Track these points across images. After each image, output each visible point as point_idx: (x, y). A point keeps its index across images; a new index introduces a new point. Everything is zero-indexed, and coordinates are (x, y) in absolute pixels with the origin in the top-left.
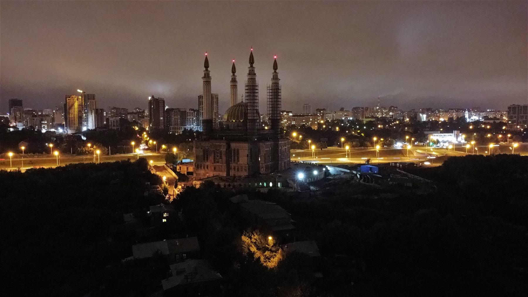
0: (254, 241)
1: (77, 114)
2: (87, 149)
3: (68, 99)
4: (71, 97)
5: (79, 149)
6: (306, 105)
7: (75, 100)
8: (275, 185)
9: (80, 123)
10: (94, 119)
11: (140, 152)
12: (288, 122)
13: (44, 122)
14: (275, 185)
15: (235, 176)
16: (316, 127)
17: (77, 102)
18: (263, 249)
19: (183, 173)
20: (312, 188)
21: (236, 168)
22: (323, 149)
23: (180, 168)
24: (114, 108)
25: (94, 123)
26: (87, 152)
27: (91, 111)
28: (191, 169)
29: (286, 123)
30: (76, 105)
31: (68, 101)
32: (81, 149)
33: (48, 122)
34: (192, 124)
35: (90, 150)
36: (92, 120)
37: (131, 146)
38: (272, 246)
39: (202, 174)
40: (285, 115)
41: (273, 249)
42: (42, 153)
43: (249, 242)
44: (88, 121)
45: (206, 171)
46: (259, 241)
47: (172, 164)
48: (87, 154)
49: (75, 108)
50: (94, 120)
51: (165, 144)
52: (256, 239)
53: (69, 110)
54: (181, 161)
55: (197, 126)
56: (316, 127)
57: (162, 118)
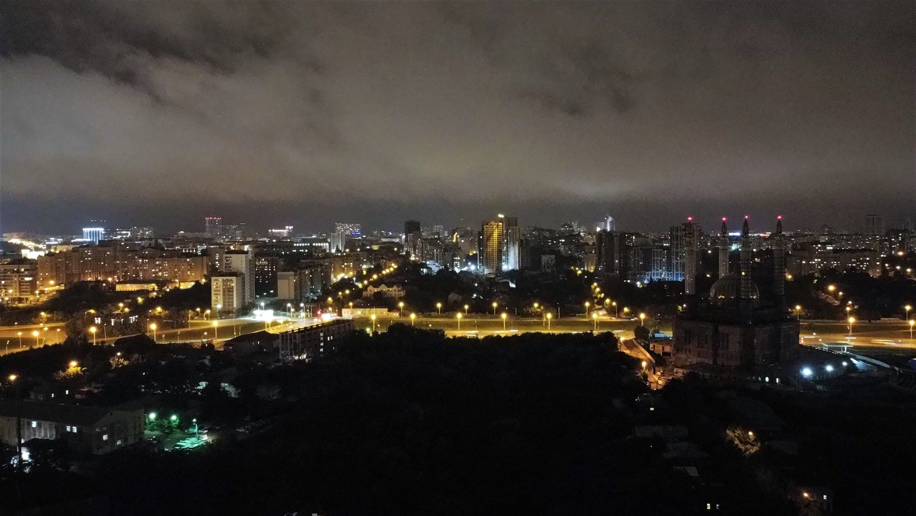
0: (738, 435)
1: (496, 247)
2: (533, 310)
3: (485, 226)
4: (489, 224)
5: (524, 309)
6: (872, 217)
7: (494, 228)
8: (772, 380)
9: (500, 260)
10: (517, 253)
11: (598, 316)
12: (823, 263)
13: (456, 258)
14: (772, 380)
15: (723, 365)
16: (878, 270)
17: (496, 230)
18: (745, 441)
19: (657, 353)
20: (819, 387)
21: (725, 355)
22: (872, 321)
23: (654, 346)
24: (535, 229)
25: (517, 259)
26: (533, 314)
27: (513, 241)
28: (668, 349)
29: (819, 263)
30: (495, 235)
31: (485, 229)
32: (527, 309)
33: (461, 258)
34: (661, 269)
35: (537, 312)
36: (515, 254)
37: (584, 307)
38: (753, 441)
39: (683, 359)
40: (819, 248)
41: (754, 443)
42: (485, 313)
43: (733, 436)
44: (508, 255)
45: (687, 355)
46: (742, 435)
47: (644, 341)
48: (534, 317)
49: (494, 239)
50: (517, 255)
51: (628, 307)
52: (739, 434)
53: (487, 241)
54: (654, 336)
55: (667, 271)
56: (878, 270)
57: (617, 261)
